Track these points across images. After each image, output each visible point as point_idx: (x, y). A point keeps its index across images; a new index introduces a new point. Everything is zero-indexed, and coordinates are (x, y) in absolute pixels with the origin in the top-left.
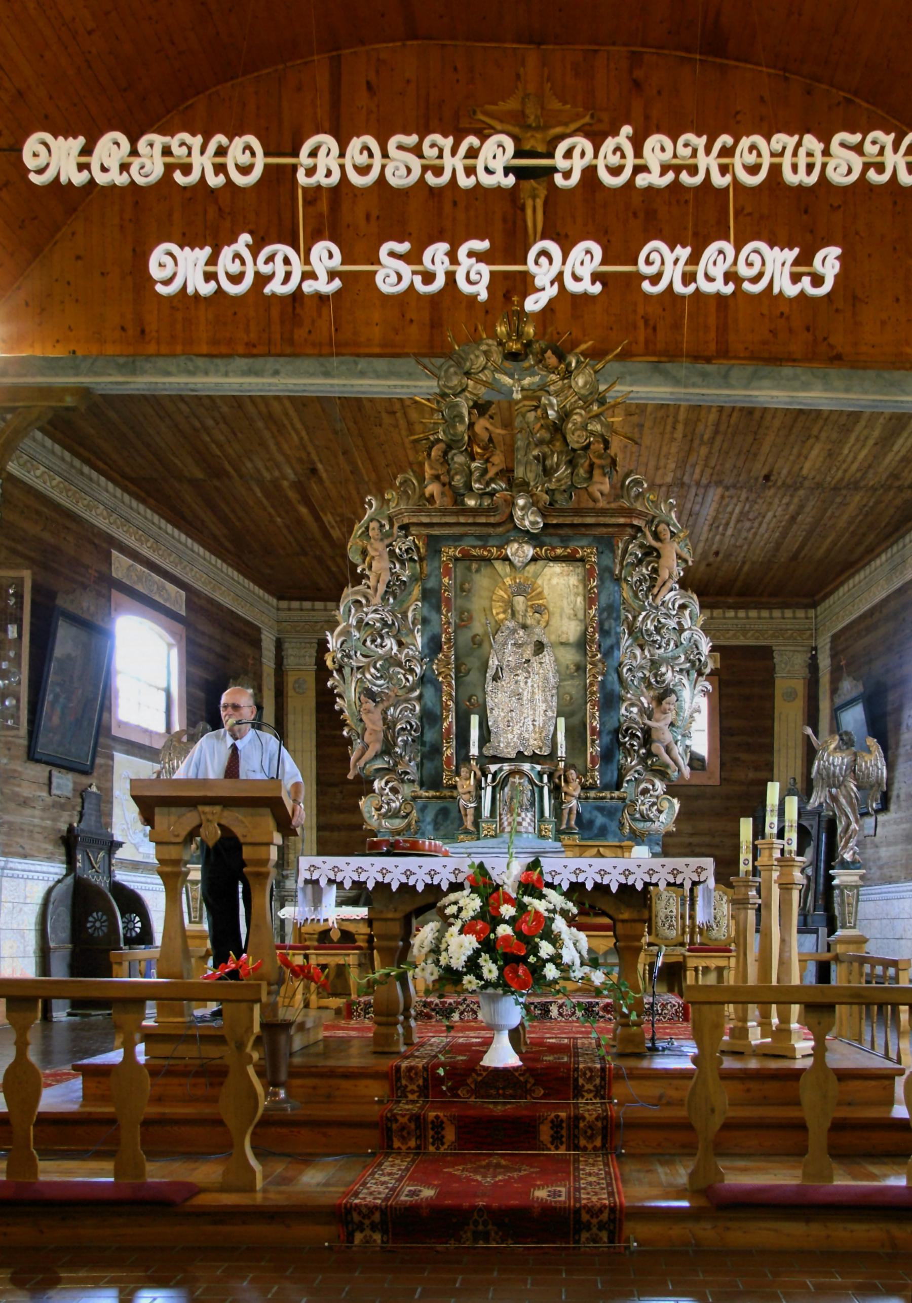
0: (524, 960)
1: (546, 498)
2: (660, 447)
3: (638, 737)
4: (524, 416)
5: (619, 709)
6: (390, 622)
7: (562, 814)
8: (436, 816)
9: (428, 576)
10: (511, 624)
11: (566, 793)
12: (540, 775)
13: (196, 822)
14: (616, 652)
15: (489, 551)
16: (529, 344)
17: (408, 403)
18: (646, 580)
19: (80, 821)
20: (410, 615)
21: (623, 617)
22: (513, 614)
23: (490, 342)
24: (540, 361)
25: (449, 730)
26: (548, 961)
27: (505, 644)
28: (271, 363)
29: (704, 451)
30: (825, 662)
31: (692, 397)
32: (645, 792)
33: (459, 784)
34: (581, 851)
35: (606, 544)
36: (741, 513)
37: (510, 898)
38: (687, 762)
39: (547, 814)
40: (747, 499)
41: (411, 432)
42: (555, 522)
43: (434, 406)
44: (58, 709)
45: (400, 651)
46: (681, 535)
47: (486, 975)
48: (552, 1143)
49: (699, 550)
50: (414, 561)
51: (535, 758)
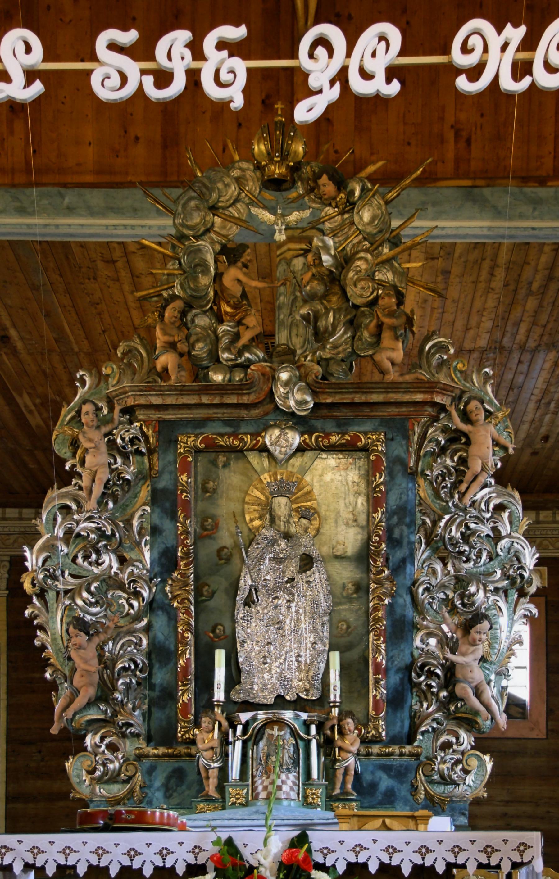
1: (318, 369)
3: (437, 675)
4: (289, 263)
5: (413, 640)
6: (109, 533)
7: (334, 775)
8: (168, 778)
9: (160, 473)
10: (269, 533)
11: (340, 749)
12: (306, 725)
14: (409, 566)
15: (242, 440)
16: (296, 168)
17: (132, 248)
18: (450, 474)
20: (135, 523)
21: (419, 522)
22: (272, 521)
23: (244, 165)
24: (312, 190)
25: (186, 668)
27: (262, 558)
29: (531, 304)
31: (519, 233)
33: (199, 739)
34: (361, 822)
35: (397, 427)
38: (503, 708)
41: (137, 287)
42: (329, 401)
43: (169, 252)
45: (121, 570)
46: (500, 415)
49: (522, 435)
51: (299, 704)
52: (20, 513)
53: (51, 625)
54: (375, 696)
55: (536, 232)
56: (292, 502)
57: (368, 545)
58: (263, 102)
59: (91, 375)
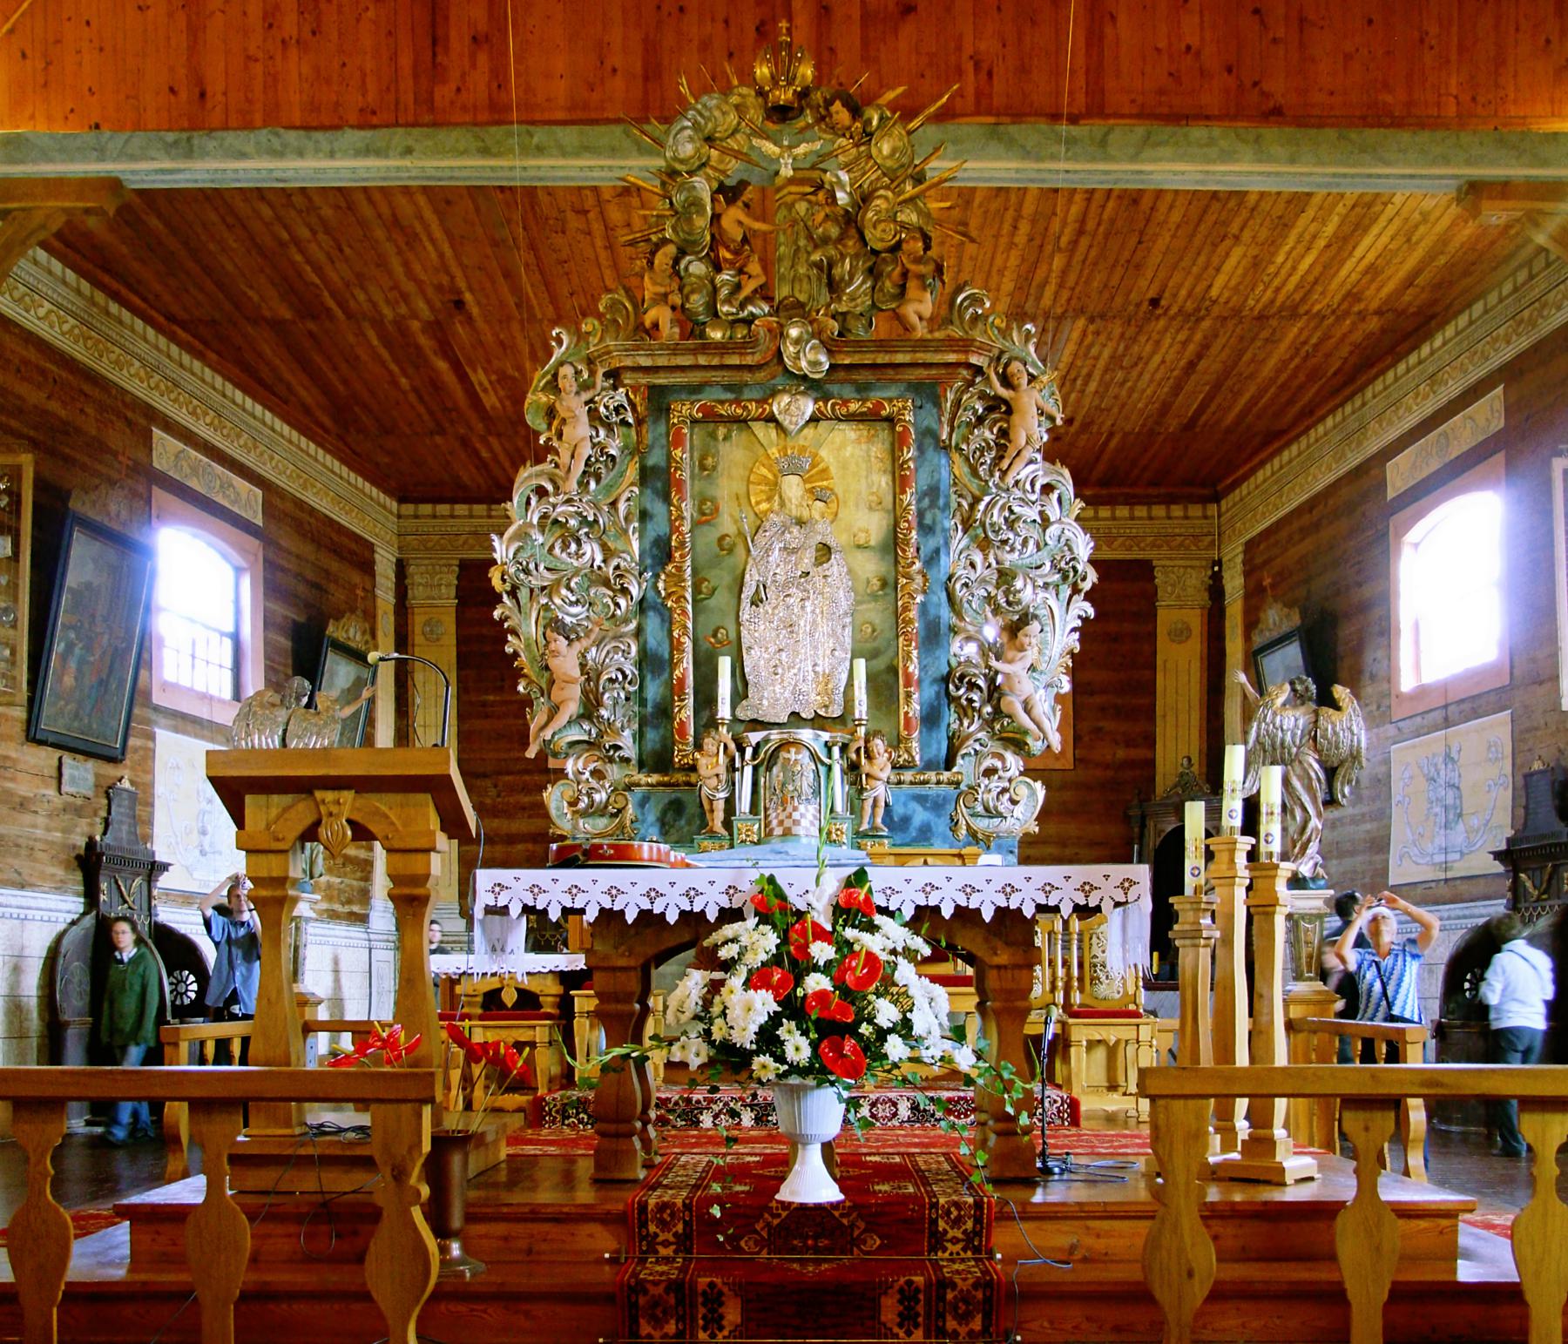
0: (852, 1030)
1: (835, 326)
2: (993, 258)
3: (979, 688)
6: (591, 518)
8: (664, 812)
12: (828, 747)
13: (309, 820)
14: (943, 557)
15: (745, 408)
18: (990, 448)
19: (105, 833)
20: (622, 506)
21: (954, 505)
23: (744, 90)
24: (823, 118)
26: (890, 1031)
28: (399, 136)
29: (1058, 262)
30: (1234, 584)
32: (990, 772)
35: (928, 393)
36: (1112, 357)
37: (823, 929)
38: (1055, 725)
39: (839, 807)
40: (1122, 335)
44: (72, 665)
47: (790, 1054)
48: (900, 1326)
50: (628, 425)
51: (818, 722)
52: (471, 510)
53: (524, 628)
54: (906, 713)
55: (1070, 176)
56: (805, 482)
57: (895, 532)
58: (757, 29)
59: (569, 332)
